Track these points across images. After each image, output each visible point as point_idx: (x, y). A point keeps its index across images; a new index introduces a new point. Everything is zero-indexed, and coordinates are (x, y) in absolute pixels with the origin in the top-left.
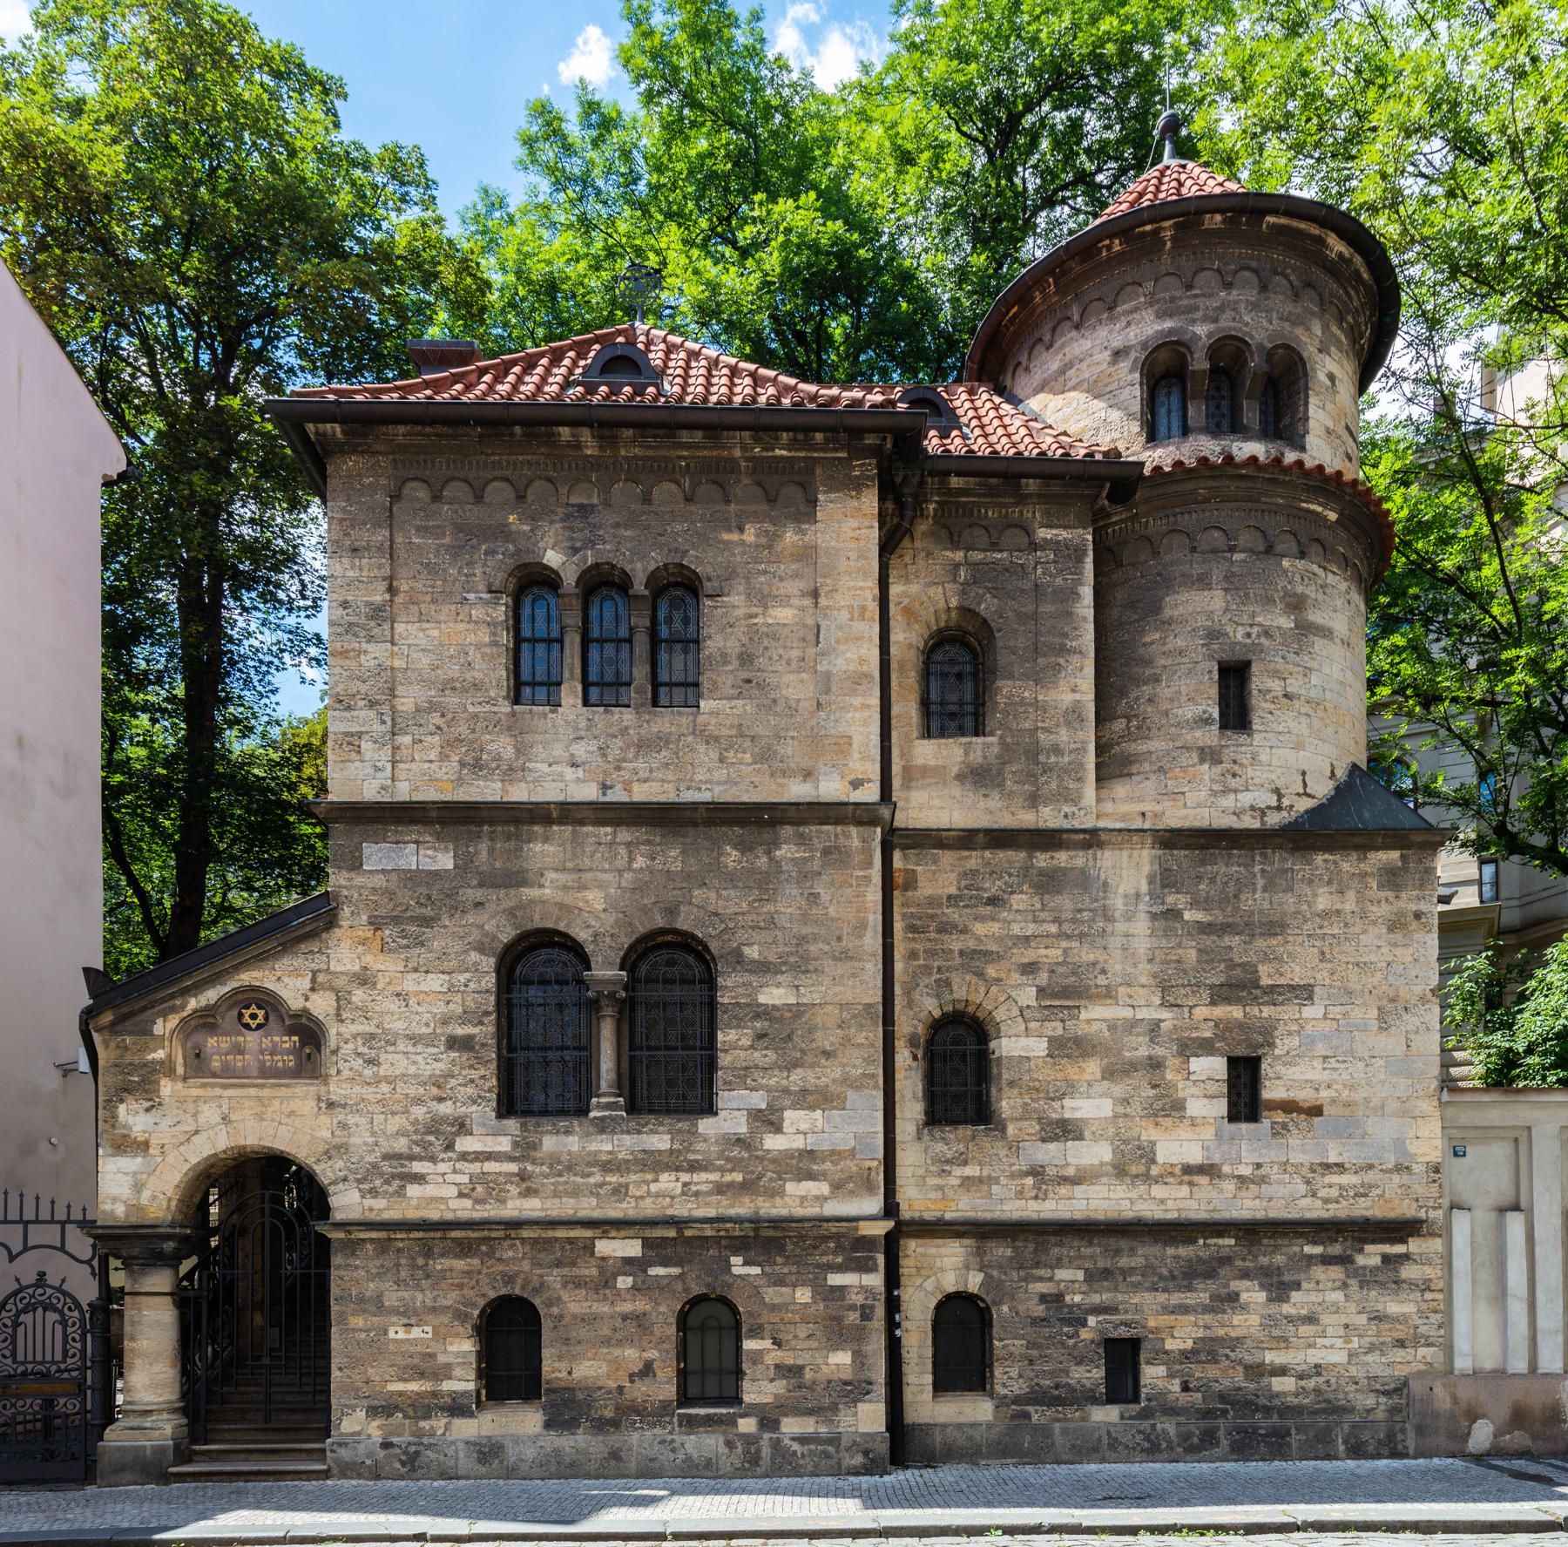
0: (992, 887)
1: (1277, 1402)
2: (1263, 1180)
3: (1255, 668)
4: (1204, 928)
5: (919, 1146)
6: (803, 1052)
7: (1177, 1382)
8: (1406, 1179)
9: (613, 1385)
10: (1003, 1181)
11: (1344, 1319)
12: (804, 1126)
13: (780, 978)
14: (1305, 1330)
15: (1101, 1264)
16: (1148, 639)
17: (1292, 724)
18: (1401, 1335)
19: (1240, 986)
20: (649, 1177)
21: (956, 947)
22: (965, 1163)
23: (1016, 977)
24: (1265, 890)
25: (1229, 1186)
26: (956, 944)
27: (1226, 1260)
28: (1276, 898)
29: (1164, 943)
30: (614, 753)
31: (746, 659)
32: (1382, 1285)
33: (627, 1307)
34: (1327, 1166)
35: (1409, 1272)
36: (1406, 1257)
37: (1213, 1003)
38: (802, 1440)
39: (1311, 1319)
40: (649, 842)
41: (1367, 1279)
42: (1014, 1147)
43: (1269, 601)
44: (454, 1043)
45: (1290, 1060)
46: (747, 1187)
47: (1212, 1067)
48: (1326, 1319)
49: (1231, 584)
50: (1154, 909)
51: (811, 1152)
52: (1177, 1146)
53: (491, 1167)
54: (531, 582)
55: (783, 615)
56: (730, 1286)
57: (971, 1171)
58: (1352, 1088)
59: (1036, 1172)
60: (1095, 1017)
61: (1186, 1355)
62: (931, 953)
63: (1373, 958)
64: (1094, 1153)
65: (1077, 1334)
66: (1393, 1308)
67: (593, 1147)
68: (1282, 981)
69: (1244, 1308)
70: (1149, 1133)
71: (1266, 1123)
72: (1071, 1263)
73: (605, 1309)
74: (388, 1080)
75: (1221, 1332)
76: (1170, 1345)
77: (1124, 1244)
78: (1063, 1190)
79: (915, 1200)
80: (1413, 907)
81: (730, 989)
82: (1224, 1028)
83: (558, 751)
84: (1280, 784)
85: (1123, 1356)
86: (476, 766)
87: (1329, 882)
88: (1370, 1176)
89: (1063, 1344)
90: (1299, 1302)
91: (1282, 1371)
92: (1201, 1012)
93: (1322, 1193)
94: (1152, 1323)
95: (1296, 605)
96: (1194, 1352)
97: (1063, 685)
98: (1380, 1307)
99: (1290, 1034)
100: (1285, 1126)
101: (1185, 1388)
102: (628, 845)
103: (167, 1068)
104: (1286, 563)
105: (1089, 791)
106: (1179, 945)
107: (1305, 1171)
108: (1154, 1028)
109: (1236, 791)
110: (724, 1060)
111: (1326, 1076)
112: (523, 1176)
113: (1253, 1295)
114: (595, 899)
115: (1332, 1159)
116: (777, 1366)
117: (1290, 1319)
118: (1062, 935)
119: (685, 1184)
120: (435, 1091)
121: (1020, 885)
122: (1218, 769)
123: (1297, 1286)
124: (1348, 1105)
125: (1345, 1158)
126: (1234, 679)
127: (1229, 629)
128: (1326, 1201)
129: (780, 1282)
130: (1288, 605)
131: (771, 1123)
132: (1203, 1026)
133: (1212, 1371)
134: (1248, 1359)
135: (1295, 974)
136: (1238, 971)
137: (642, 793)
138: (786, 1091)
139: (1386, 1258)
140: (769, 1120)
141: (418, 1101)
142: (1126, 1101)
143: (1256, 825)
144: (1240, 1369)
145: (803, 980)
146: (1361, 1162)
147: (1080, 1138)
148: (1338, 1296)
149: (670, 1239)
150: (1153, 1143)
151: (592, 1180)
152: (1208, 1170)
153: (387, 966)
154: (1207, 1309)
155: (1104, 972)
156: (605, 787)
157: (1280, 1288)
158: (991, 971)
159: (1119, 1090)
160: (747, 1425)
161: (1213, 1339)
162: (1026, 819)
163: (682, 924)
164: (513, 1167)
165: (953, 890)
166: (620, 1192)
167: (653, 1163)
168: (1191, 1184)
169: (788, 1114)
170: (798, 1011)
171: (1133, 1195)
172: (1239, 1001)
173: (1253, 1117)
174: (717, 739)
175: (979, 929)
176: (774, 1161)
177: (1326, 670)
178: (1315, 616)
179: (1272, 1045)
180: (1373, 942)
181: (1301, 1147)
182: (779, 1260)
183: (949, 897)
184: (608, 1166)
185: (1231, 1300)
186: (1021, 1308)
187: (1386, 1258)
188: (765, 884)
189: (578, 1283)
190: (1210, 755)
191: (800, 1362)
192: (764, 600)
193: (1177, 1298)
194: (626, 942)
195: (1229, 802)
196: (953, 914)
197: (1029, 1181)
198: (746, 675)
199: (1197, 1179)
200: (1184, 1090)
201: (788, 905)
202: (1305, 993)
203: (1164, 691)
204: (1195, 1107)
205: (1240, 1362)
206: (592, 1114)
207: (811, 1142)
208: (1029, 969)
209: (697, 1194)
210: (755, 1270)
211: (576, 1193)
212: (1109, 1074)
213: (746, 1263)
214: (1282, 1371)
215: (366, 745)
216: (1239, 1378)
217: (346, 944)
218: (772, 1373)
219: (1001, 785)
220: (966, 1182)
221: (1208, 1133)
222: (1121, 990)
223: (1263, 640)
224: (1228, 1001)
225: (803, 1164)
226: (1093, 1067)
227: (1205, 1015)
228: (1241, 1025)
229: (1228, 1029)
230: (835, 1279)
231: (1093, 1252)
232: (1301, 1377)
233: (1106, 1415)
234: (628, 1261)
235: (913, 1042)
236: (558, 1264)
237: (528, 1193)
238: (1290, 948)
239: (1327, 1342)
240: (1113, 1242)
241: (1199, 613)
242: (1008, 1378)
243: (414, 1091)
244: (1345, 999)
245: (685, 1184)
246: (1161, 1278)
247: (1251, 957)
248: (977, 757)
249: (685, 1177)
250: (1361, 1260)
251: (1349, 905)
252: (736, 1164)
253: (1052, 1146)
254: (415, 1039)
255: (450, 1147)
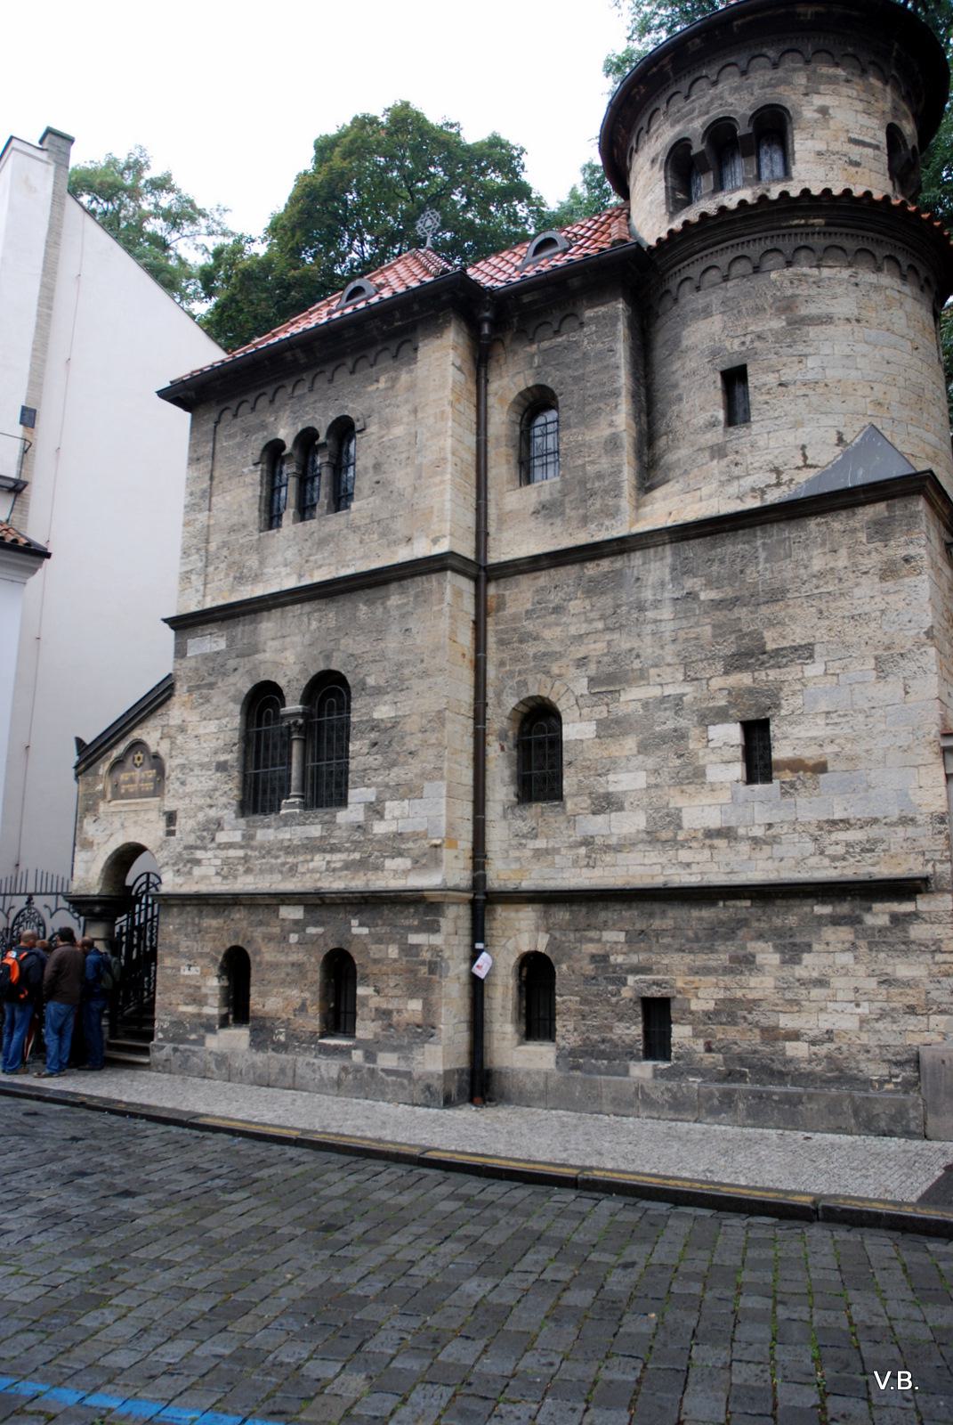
0: (555, 598)
1: (791, 1067)
2: (774, 841)
3: (750, 370)
4: (717, 604)
5: (504, 824)
6: (398, 753)
7: (701, 1042)
8: (911, 831)
9: (284, 1016)
10: (563, 851)
11: (854, 983)
12: (397, 813)
13: (386, 698)
14: (816, 993)
15: (638, 926)
16: (674, 368)
17: (787, 407)
18: (913, 1001)
19: (749, 655)
20: (309, 857)
21: (531, 652)
22: (536, 837)
23: (573, 671)
24: (767, 560)
25: (744, 847)
26: (531, 649)
27: (743, 923)
28: (776, 566)
29: (685, 623)
30: (306, 552)
31: (377, 467)
32: (891, 945)
33: (294, 957)
34: (834, 823)
35: (917, 931)
36: (915, 916)
37: (726, 673)
38: (388, 1072)
39: (821, 983)
40: (319, 610)
41: (877, 940)
42: (571, 820)
43: (758, 310)
44: (222, 767)
45: (796, 718)
46: (362, 865)
47: (732, 733)
48: (837, 982)
49: (728, 306)
50: (676, 596)
51: (401, 834)
52: (700, 812)
53: (232, 853)
54: (274, 451)
55: (398, 430)
56: (349, 942)
57: (541, 843)
58: (854, 740)
59: (587, 842)
60: (632, 698)
61: (709, 1016)
62: (515, 660)
63: (867, 608)
64: (631, 822)
65: (618, 993)
66: (903, 970)
67: (281, 836)
68: (785, 644)
69: (760, 970)
70: (676, 800)
71: (776, 782)
72: (614, 927)
73: (283, 958)
74: (190, 795)
75: (739, 994)
76: (695, 1005)
77: (656, 907)
78: (608, 858)
79: (500, 874)
80: (903, 552)
81: (360, 710)
82: (735, 695)
83: (279, 558)
84: (777, 463)
85: (657, 1013)
86: (240, 579)
87: (823, 544)
88: (874, 831)
89: (608, 1001)
90: (811, 964)
91: (795, 1036)
92: (717, 683)
93: (830, 851)
94: (680, 984)
95: (786, 306)
96: (717, 1012)
97: (603, 421)
98: (889, 970)
99: (794, 693)
100: (792, 785)
101: (709, 1049)
102: (309, 613)
103: (103, 795)
104: (773, 275)
105: (626, 503)
106: (697, 624)
107: (813, 830)
108: (677, 703)
109: (738, 478)
110: (353, 765)
111: (829, 731)
112: (246, 859)
113: (768, 956)
114: (290, 657)
115: (837, 817)
116: (377, 1009)
117: (802, 982)
118: (607, 629)
119: (328, 862)
120: (209, 801)
121: (575, 592)
122: (725, 462)
123: (808, 948)
124: (850, 759)
125: (850, 814)
126: (734, 379)
127: (728, 344)
128: (834, 858)
129: (379, 941)
130: (778, 309)
131: (378, 813)
132: (718, 695)
133: (732, 1033)
134: (764, 1022)
135: (797, 635)
136: (746, 640)
137: (319, 576)
138: (387, 786)
139: (896, 919)
140: (375, 809)
141: (201, 808)
142: (656, 771)
143: (756, 504)
144: (757, 1031)
145: (401, 697)
146: (866, 816)
147: (621, 809)
148: (846, 959)
149: (317, 903)
150: (680, 810)
151: (279, 861)
152: (726, 833)
153: (192, 717)
154: (727, 971)
155: (638, 656)
156: (300, 576)
157: (793, 951)
158: (555, 670)
159: (651, 762)
160: (357, 1056)
161: (732, 1001)
162: (582, 538)
163: (334, 667)
164: (241, 853)
165: (529, 606)
166: (293, 870)
167: (312, 847)
168: (711, 847)
169: (388, 804)
170: (395, 723)
171: (663, 860)
172: (747, 667)
173: (767, 779)
174: (359, 527)
175: (547, 634)
176: (379, 841)
177: (826, 350)
178: (804, 311)
179: (778, 706)
180: (866, 593)
181: (809, 807)
182: (380, 922)
183: (527, 612)
184: (289, 850)
185: (745, 962)
186: (577, 966)
187: (896, 919)
188: (379, 631)
189: (269, 938)
190: (718, 452)
191: (390, 1007)
192: (387, 424)
193: (701, 960)
194: (304, 683)
195: (733, 489)
196: (529, 626)
197: (583, 851)
198: (376, 478)
199: (717, 842)
200: (706, 758)
201: (392, 643)
202: (805, 652)
203: (685, 406)
204: (715, 774)
205: (757, 1025)
206: (283, 812)
207: (406, 827)
208: (582, 662)
209: (334, 870)
210: (365, 931)
211: (271, 870)
212: (643, 748)
213: (361, 925)
214: (795, 1036)
215: (193, 577)
216: (755, 1038)
217: (176, 707)
218: (373, 1015)
219: (563, 513)
220: (539, 854)
221: (724, 797)
222: (653, 671)
223: (757, 344)
224: (739, 669)
225: (395, 844)
226: (630, 743)
227: (721, 683)
228: (750, 691)
229: (739, 696)
230: (414, 939)
231: (631, 916)
232: (813, 1043)
233: (642, 1070)
234: (296, 922)
235: (502, 736)
236: (261, 923)
237: (248, 871)
238: (790, 611)
239: (838, 1006)
240: (648, 907)
241: (705, 331)
242: (567, 1029)
243: (201, 802)
244: (844, 653)
245: (328, 862)
246: (688, 940)
247: (757, 626)
248: (545, 497)
249: (328, 857)
250: (869, 920)
251: (842, 561)
252: (357, 845)
253: (600, 819)
254: (202, 766)
255: (213, 840)
